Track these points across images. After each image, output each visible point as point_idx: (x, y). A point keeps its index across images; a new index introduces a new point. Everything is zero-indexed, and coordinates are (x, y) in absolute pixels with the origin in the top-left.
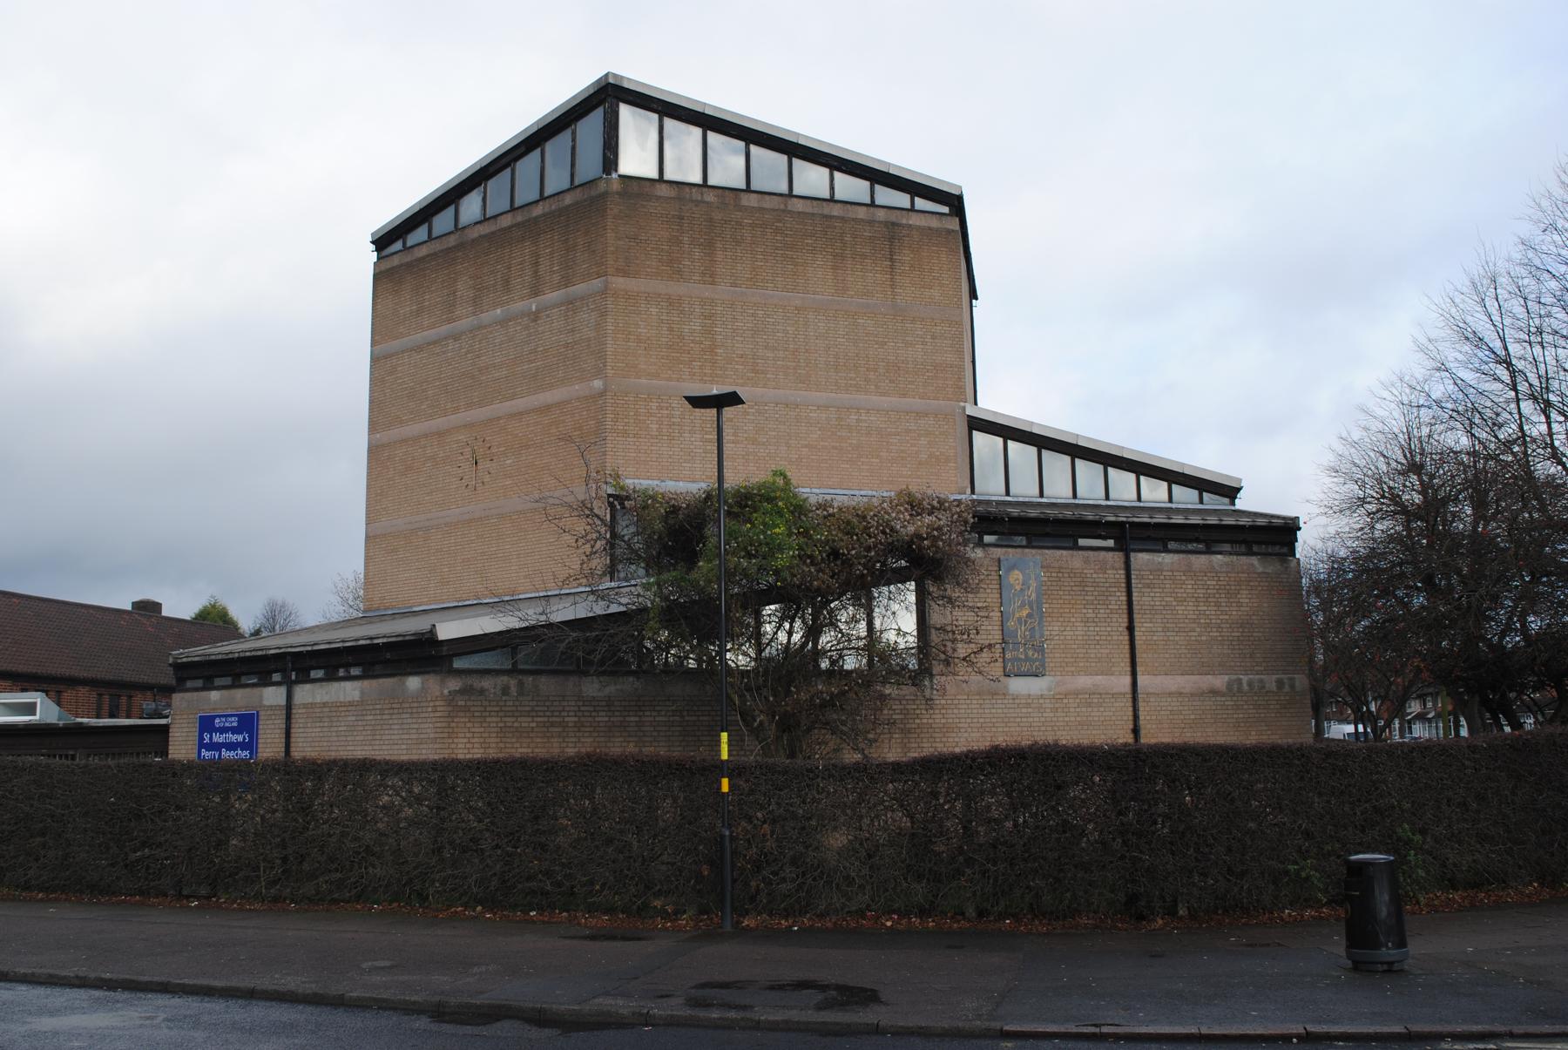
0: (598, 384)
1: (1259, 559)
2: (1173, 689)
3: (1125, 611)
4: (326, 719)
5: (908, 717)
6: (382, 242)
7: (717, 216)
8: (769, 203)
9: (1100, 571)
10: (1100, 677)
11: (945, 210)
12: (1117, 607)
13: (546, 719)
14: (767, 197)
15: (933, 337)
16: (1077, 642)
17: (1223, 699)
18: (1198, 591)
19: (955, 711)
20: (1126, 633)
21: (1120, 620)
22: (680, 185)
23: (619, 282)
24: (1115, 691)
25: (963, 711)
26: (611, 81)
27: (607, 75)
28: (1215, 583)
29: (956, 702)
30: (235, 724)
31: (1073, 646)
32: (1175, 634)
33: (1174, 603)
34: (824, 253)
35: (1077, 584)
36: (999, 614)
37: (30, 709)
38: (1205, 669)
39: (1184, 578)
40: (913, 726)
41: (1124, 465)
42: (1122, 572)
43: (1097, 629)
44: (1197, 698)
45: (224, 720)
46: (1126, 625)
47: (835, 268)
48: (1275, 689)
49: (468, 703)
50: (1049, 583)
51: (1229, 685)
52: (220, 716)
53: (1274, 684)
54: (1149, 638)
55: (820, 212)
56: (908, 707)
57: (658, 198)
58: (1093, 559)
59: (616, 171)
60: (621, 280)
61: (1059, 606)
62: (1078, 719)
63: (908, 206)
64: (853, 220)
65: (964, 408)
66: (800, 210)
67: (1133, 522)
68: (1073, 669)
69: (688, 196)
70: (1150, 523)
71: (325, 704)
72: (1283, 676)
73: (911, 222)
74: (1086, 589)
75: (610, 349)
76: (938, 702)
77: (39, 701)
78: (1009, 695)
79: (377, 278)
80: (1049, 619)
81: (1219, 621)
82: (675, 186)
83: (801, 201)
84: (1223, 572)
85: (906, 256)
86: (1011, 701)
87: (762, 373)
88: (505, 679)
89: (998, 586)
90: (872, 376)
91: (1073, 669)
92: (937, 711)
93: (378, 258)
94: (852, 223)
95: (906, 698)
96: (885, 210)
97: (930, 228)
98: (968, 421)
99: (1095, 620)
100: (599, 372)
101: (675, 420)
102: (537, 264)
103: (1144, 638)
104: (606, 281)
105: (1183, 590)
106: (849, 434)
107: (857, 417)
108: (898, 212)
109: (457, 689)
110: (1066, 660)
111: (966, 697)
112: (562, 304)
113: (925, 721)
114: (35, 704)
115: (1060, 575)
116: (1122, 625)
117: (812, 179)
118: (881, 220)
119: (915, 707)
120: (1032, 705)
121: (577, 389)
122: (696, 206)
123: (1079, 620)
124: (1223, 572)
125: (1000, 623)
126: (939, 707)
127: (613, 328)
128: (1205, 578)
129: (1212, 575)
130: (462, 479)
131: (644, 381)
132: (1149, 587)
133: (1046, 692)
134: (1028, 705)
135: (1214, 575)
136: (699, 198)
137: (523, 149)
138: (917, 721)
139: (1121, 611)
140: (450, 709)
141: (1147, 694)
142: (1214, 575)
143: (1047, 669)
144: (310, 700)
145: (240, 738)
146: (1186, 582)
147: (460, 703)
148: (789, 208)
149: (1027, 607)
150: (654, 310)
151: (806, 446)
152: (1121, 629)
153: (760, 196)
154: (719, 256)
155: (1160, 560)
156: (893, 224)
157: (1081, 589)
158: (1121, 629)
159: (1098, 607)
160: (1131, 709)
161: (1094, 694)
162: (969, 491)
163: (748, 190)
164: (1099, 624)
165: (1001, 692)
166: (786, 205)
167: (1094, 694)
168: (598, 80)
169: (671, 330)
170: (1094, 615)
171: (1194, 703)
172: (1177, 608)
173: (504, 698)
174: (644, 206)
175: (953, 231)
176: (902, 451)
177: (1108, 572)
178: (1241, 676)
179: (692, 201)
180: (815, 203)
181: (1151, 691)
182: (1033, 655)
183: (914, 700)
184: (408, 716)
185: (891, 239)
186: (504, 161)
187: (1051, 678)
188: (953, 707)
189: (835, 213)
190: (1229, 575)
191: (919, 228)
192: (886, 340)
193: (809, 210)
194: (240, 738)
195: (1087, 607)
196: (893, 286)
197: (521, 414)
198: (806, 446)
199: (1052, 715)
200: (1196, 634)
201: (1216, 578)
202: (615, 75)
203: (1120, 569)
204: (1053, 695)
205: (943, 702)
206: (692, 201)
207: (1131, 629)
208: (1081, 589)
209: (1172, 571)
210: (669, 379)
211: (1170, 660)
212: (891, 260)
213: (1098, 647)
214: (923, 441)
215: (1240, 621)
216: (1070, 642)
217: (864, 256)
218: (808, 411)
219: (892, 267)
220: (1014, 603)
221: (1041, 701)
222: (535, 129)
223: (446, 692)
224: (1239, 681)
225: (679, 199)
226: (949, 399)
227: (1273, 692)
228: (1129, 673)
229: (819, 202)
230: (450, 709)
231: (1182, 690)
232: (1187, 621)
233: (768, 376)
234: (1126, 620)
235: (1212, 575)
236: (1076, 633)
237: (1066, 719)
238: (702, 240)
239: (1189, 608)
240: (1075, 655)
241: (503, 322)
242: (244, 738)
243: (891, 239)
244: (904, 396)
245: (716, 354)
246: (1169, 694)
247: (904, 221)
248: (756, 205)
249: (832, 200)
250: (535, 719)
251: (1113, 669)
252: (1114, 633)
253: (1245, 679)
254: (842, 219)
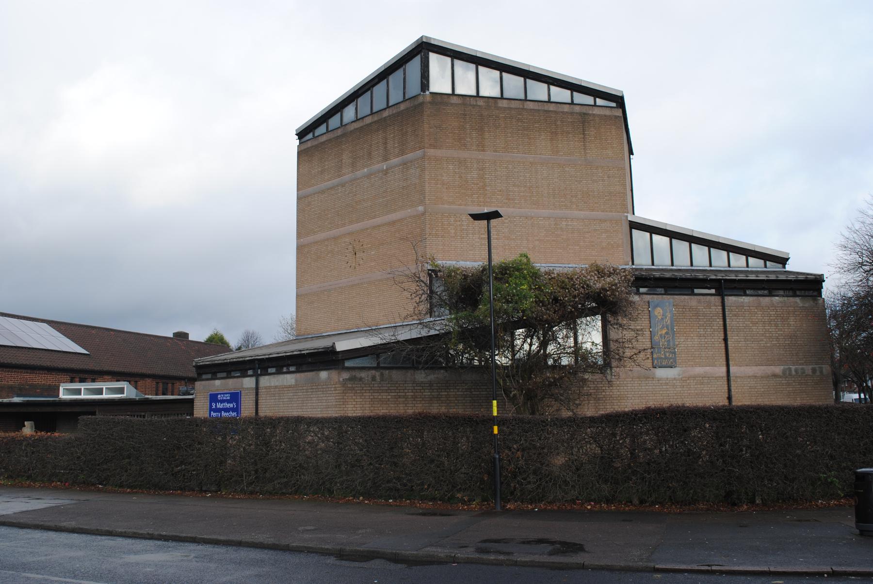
0: (421, 208)
1: (800, 299)
2: (751, 374)
3: (722, 330)
4: (277, 395)
5: (598, 391)
6: (302, 134)
7: (485, 113)
8: (514, 104)
9: (707, 307)
10: (708, 368)
12: (718, 328)
13: (396, 394)
14: (513, 102)
15: (609, 177)
16: (694, 348)
17: (780, 379)
18: (764, 318)
19: (625, 388)
20: (723, 342)
21: (719, 335)
22: (464, 97)
23: (431, 152)
24: (717, 375)
25: (629, 388)
26: (424, 40)
27: (422, 37)
28: (774, 313)
29: (625, 382)
30: (228, 398)
31: (692, 350)
32: (751, 342)
33: (751, 325)
34: (546, 132)
35: (694, 315)
36: (649, 333)
37: (121, 390)
38: (769, 363)
39: (756, 310)
40: (601, 396)
41: (720, 247)
42: (720, 308)
43: (706, 340)
44: (765, 379)
45: (223, 396)
46: (723, 338)
47: (552, 140)
48: (811, 374)
49: (354, 386)
50: (678, 315)
51: (784, 371)
52: (220, 394)
53: (810, 371)
54: (736, 345)
55: (543, 109)
56: (598, 385)
57: (452, 104)
58: (703, 301)
59: (428, 90)
60: (432, 150)
61: (684, 328)
62: (696, 392)
63: (592, 103)
65: (627, 217)
66: (532, 108)
67: (726, 279)
68: (693, 363)
69: (468, 103)
70: (736, 279)
71: (276, 387)
72: (815, 366)
73: (594, 113)
74: (699, 317)
75: (427, 189)
76: (615, 383)
77: (125, 386)
78: (656, 378)
79: (300, 154)
80: (678, 335)
81: (777, 335)
82: (461, 97)
83: (532, 103)
84: (779, 307)
85: (591, 132)
86: (657, 382)
87: (512, 200)
88: (373, 372)
89: (648, 317)
90: (574, 200)
91: (693, 363)
92: (615, 388)
93: (300, 143)
94: (561, 114)
95: (597, 380)
96: (579, 106)
97: (605, 116)
98: (629, 224)
99: (705, 335)
100: (422, 202)
101: (464, 227)
102: (386, 143)
103: (733, 345)
104: (425, 152)
105: (755, 318)
106: (562, 233)
107: (566, 223)
108: (587, 107)
109: (347, 377)
110: (688, 358)
111: (631, 380)
112: (400, 165)
113: (607, 393)
114: (81, 389)
115: (684, 310)
116: (721, 338)
117: (539, 91)
118: (578, 112)
119: (602, 386)
120: (670, 384)
121: (409, 212)
122: (473, 108)
123: (695, 335)
124: (779, 307)
125: (650, 338)
126: (616, 385)
127: (429, 177)
128: (769, 310)
129: (773, 308)
130: (347, 263)
131: (446, 206)
132: (736, 316)
133: (677, 377)
134: (667, 384)
135: (774, 308)
136: (475, 104)
137: (376, 80)
138: (604, 393)
139: (719, 330)
140: (344, 389)
141: (736, 377)
142: (774, 308)
143: (677, 363)
144: (269, 385)
145: (231, 406)
146: (758, 313)
147: (349, 385)
148: (525, 107)
149: (665, 328)
150: (451, 167)
151: (538, 240)
152: (720, 340)
153: (508, 101)
154: (487, 135)
155: (742, 300)
156: (584, 114)
157: (696, 317)
158: (720, 340)
159: (706, 327)
160: (726, 386)
161: (705, 377)
162: (630, 263)
163: (502, 98)
164: (707, 338)
165: (651, 377)
166: (524, 106)
167: (705, 377)
168: (417, 40)
169: (460, 177)
170: (704, 333)
171: (764, 382)
172: (752, 328)
173: (373, 383)
174: (444, 109)
175: (618, 116)
176: (592, 242)
177: (712, 308)
178: (791, 366)
179: (471, 105)
180: (540, 103)
181: (737, 375)
182: (669, 355)
183: (601, 382)
184: (321, 393)
185: (583, 122)
186: (367, 87)
187: (679, 369)
188: (623, 385)
189: (552, 109)
190: (783, 308)
192: (582, 179)
193: (536, 108)
194: (231, 406)
195: (700, 327)
196: (585, 149)
197: (379, 226)
198: (538, 240)
199: (680, 389)
200: (764, 342)
201: (775, 310)
202: (426, 37)
203: (719, 306)
204: (681, 378)
205: (618, 382)
206: (471, 105)
207: (726, 340)
208: (696, 317)
209: (750, 307)
210: (460, 205)
211: (749, 357)
212: (584, 134)
213: (707, 350)
214: (604, 236)
215: (790, 335)
216: (690, 348)
217: (568, 133)
218: (538, 220)
219: (584, 138)
220: (658, 326)
221: (675, 382)
222: (383, 69)
223: (341, 379)
224: (790, 369)
225: (464, 104)
226: (618, 212)
227: (810, 375)
228: (725, 365)
229: (542, 103)
230: (344, 389)
231: (756, 375)
232: (758, 335)
233: (515, 201)
234: (723, 335)
235: (773, 308)
236: (694, 343)
237: (689, 392)
238: (477, 127)
239: (759, 328)
240: (693, 355)
241: (368, 176)
242: (234, 406)
243: (583, 122)
244: (593, 210)
245: (486, 190)
246: (749, 377)
247: (591, 112)
248: (506, 106)
249: (549, 102)
250: (390, 394)
251: (716, 363)
252: (715, 343)
253: (793, 368)
254: (556, 112)
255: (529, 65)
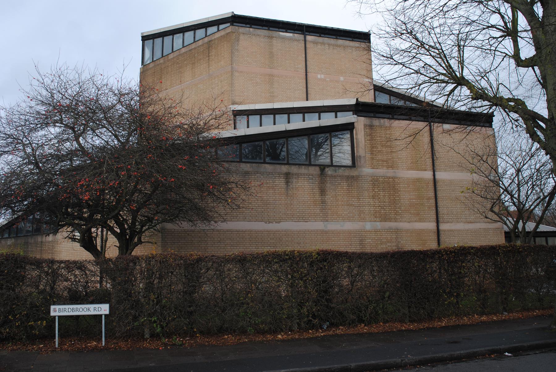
11: (229, 24)
15: (221, 82)
64: (198, 47)
191: (218, 38)
217: (200, 59)
254: (195, 48)
255: (183, 23)
